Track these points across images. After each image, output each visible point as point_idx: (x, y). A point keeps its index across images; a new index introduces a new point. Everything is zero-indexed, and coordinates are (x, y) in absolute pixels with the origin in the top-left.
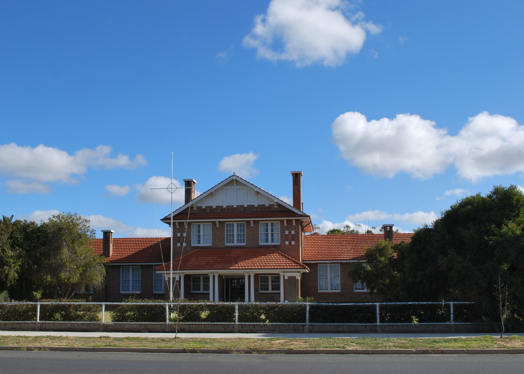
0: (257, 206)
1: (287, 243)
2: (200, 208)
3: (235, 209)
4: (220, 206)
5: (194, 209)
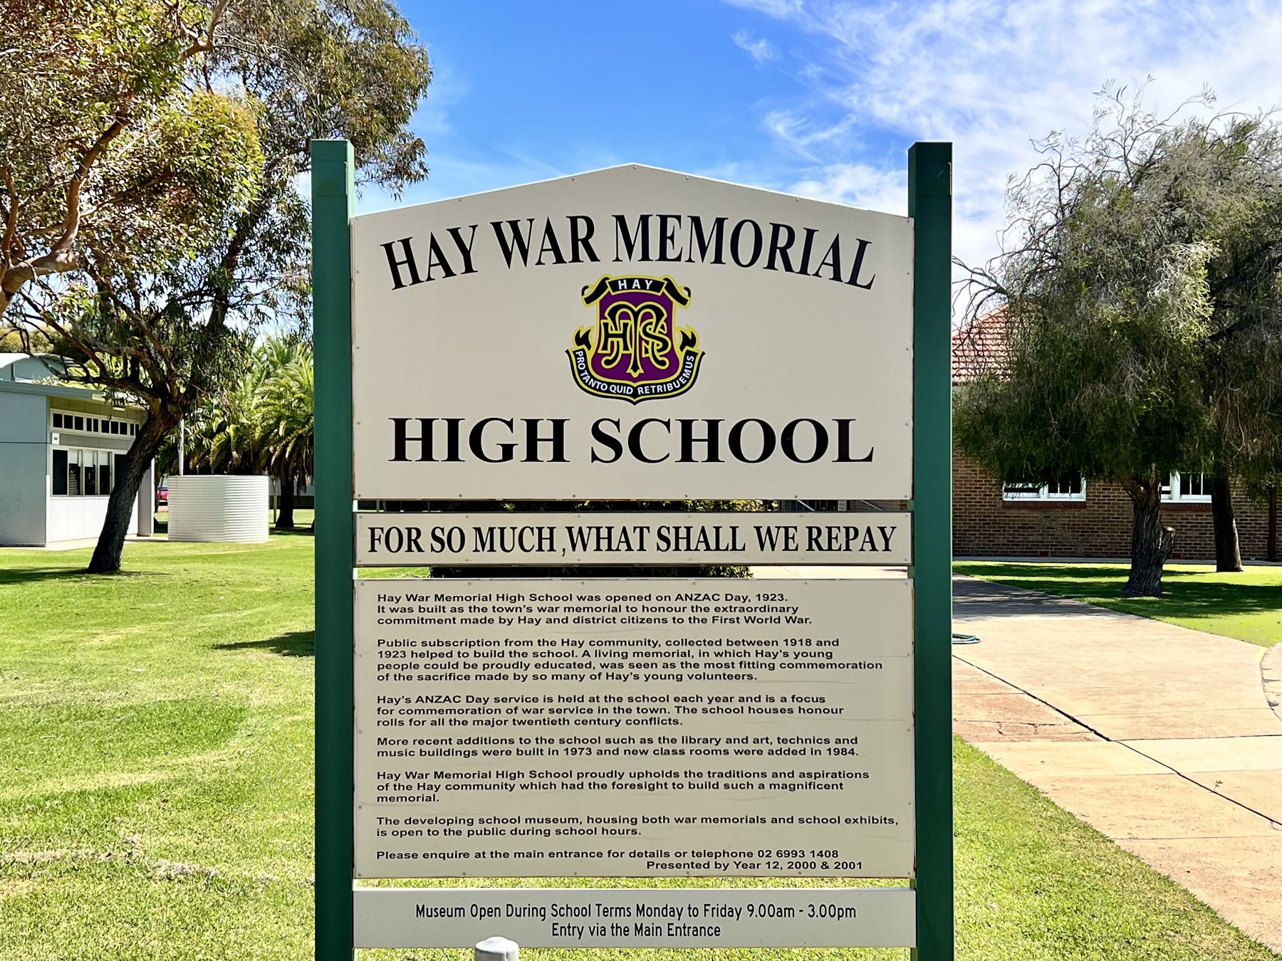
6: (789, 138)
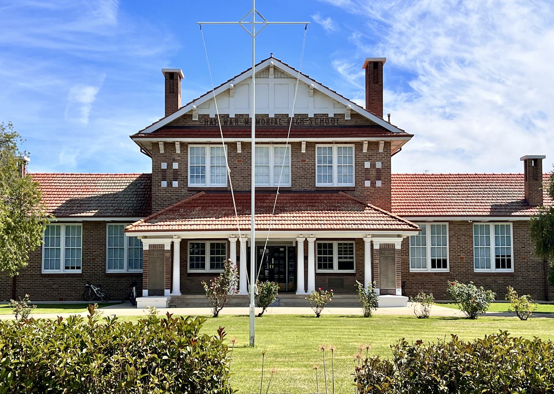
0: (234, 117)
1: (367, 184)
2: (204, 117)
3: (272, 121)
4: (242, 115)
5: (193, 119)
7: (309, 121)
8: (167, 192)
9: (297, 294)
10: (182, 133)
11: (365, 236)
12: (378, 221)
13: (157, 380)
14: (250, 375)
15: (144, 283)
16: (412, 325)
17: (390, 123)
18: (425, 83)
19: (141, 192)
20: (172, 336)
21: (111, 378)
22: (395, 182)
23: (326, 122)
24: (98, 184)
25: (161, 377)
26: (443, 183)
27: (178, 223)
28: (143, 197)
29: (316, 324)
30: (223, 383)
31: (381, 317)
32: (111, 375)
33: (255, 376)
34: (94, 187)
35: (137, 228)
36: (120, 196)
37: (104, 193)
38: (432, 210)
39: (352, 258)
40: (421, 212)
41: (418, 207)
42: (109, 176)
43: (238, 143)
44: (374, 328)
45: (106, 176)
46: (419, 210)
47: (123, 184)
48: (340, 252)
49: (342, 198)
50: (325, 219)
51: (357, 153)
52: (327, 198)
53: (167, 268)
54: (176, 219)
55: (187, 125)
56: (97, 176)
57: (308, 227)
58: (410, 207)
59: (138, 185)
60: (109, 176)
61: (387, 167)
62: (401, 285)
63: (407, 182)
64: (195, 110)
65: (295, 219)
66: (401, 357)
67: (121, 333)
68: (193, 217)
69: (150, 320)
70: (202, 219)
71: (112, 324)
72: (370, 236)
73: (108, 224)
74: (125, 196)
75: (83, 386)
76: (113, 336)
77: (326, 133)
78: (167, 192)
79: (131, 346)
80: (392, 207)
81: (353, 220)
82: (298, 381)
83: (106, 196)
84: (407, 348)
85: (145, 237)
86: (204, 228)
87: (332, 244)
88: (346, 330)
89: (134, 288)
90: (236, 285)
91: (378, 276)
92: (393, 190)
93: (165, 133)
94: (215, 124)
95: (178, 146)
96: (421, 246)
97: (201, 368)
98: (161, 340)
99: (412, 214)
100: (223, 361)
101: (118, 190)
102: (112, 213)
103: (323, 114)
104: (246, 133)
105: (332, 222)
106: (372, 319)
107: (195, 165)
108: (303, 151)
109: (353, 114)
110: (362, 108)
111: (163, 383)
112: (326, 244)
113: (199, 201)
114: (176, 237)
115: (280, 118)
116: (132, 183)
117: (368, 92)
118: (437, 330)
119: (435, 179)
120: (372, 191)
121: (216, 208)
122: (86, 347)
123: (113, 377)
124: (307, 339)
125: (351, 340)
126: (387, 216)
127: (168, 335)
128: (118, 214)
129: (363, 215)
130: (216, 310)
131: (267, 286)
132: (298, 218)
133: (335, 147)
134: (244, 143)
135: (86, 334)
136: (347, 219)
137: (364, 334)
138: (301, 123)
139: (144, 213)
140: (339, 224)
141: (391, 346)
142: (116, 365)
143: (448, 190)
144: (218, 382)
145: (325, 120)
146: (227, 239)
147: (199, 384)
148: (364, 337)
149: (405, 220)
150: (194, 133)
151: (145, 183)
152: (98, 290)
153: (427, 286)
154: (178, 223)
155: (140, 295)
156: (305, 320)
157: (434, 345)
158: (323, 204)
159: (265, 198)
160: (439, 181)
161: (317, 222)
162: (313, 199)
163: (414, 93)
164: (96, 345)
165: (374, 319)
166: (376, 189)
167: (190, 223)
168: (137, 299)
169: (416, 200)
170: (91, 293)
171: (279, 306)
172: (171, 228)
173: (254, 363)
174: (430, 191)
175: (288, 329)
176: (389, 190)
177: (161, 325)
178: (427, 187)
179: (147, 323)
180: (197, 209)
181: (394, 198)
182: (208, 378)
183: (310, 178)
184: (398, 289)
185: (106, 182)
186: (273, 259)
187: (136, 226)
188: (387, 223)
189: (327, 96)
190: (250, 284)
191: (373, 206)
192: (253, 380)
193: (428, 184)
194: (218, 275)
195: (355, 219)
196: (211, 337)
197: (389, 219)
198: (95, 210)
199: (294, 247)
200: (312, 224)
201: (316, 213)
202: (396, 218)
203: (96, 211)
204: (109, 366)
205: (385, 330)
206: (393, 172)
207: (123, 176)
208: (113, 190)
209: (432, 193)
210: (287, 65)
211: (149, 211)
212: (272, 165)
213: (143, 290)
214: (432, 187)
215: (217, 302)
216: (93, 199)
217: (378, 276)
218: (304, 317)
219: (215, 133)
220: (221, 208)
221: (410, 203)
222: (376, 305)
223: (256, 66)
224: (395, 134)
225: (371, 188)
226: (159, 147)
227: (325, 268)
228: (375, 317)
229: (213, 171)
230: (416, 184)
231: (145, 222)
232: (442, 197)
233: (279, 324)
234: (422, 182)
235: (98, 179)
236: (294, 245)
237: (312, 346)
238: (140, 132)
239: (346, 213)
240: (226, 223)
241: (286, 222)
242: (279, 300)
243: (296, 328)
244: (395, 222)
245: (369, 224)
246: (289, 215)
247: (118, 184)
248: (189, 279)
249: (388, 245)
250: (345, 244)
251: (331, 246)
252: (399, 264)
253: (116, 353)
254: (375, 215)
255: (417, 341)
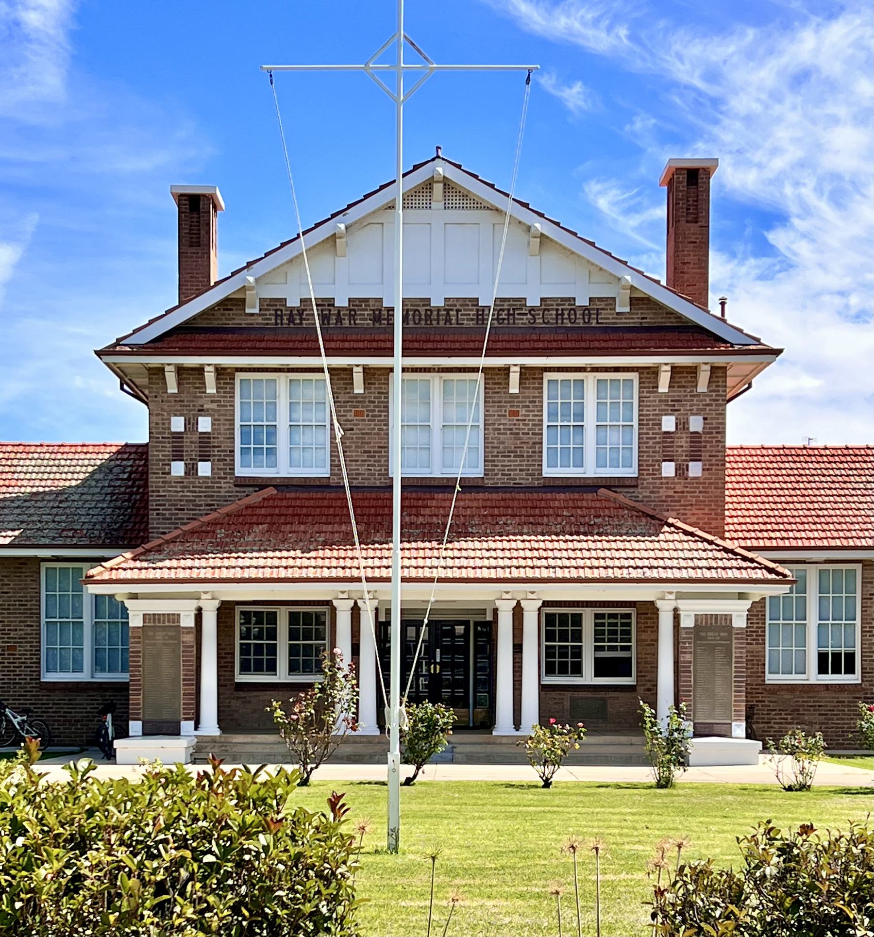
1: (668, 469)
2: (275, 305)
3: (438, 315)
4: (366, 300)
5: (248, 311)
6: (615, 216)
7: (529, 316)
8: (186, 487)
9: (494, 733)
10: (221, 344)
11: (660, 596)
12: (692, 559)
13: (191, 910)
14: (393, 914)
15: (133, 704)
16: (771, 805)
17: (724, 321)
18: (804, 236)
19: (123, 489)
20: (223, 810)
21: (83, 904)
22: (735, 466)
23: (570, 319)
24: (19, 469)
25: (199, 903)
26: (851, 469)
27: (211, 563)
28: (129, 500)
29: (541, 803)
30: (342, 921)
31: (696, 788)
32: (84, 896)
33: (404, 916)
34: (9, 476)
35: (114, 575)
36: (72, 498)
37: (34, 490)
38: (823, 535)
39: (628, 648)
40: (796, 538)
41: (788, 527)
42: (45, 449)
43: (355, 369)
44: (681, 811)
45: (39, 450)
46: (791, 534)
47: (78, 469)
48: (599, 635)
49: (607, 504)
50: (565, 554)
51: (645, 394)
52: (571, 504)
53: (188, 670)
54: (208, 553)
55: (231, 324)
56: (15, 449)
57: (523, 575)
58: (769, 527)
59: (116, 470)
60: (45, 449)
61: (716, 429)
62: (744, 713)
63: (764, 465)
64: (251, 288)
65: (493, 553)
66: (763, 862)
67: (105, 802)
68: (248, 548)
69: (169, 775)
70: (270, 554)
71: (82, 781)
72: (673, 597)
73: (44, 566)
74: (84, 497)
75: (17, 922)
76: (88, 807)
77: (569, 345)
78: (186, 487)
79: (128, 833)
80: (726, 528)
81: (633, 559)
82: (506, 930)
83: (39, 498)
84: (778, 844)
85: (134, 596)
86: (275, 576)
87: (581, 615)
88: (616, 817)
89: (109, 717)
90: (353, 710)
91: (690, 691)
92: (730, 486)
93: (180, 344)
94: (301, 324)
95: (210, 377)
96: (794, 622)
97: (294, 886)
98: (198, 820)
99: (774, 543)
100: (343, 869)
101: (67, 483)
102: (54, 538)
103: (563, 299)
104: (374, 345)
105: (581, 563)
106: (675, 792)
107: (252, 423)
108: (514, 389)
109: (637, 299)
110: (658, 282)
111: (205, 918)
112: (566, 615)
113: (263, 511)
114: (208, 596)
115: (458, 307)
116: (100, 466)
117: (672, 243)
118: (832, 818)
119: (831, 459)
120: (679, 488)
121: (302, 528)
122: (24, 832)
123: (89, 902)
124: (523, 837)
125: (626, 840)
126: (714, 547)
127: (215, 807)
128: (69, 540)
129: (657, 545)
130: (305, 769)
131: (426, 713)
132: (500, 554)
133: (590, 380)
134: (370, 369)
135: (24, 803)
136: (617, 554)
137: (658, 825)
138: (508, 319)
139: (131, 539)
140: (597, 568)
141: (738, 839)
142: (95, 874)
143: (862, 486)
144: (330, 918)
145: (566, 312)
146: (328, 603)
147: (288, 921)
148: (657, 832)
149: (760, 557)
150: (249, 344)
151: (131, 466)
152: (23, 721)
153: (806, 718)
154: (211, 563)
155: (123, 733)
156: (516, 792)
157: (841, 837)
158: (559, 519)
159: (420, 503)
160: (841, 462)
161: (544, 563)
162: (536, 507)
163: (779, 259)
164: (46, 829)
165: (681, 792)
166: (689, 483)
167: (240, 562)
168: (117, 744)
169: (784, 509)
170: (6, 728)
171: (452, 761)
172: (195, 574)
173: (400, 888)
174: (818, 489)
175: (476, 814)
176: (720, 485)
177: (198, 785)
178: (811, 479)
179: (163, 780)
180: (256, 529)
181: (731, 506)
182: (308, 908)
183: (531, 456)
184: (738, 723)
185: (39, 462)
186: (438, 650)
187: (112, 569)
188: (713, 564)
189: (573, 253)
190: (389, 706)
191: (680, 524)
192: (400, 926)
193: (814, 472)
194: (311, 686)
195: (637, 554)
196: (314, 815)
197: (719, 555)
198: (13, 530)
199: (489, 623)
200: (532, 568)
201: (544, 541)
202: (736, 554)
203: (17, 533)
204: (78, 878)
205: (707, 817)
206: (731, 440)
207: (79, 449)
208: (56, 483)
209: (822, 492)
210: (476, 177)
211: (142, 534)
212: (436, 423)
213: (131, 723)
214: (823, 479)
215: (306, 751)
216: (8, 503)
217: (690, 691)
218: (512, 786)
219: (299, 345)
220: (316, 528)
221: (769, 517)
222: (682, 761)
223: (404, 175)
224: (736, 348)
225: (676, 480)
226: (164, 378)
227: (563, 671)
228: (684, 788)
229: (296, 438)
230: (784, 472)
231: (134, 559)
232: (848, 502)
233: (456, 801)
234: (799, 465)
235: (19, 456)
236: (489, 618)
237: (532, 851)
238: (118, 342)
239: (615, 541)
240: (327, 563)
241: (471, 563)
242: (453, 747)
243: (495, 812)
244: (734, 563)
245: (671, 568)
246: (478, 545)
247: (66, 469)
248: (238, 698)
249: (716, 619)
250: (611, 616)
251: (577, 620)
252: (742, 662)
253: (95, 846)
254: (686, 545)
255: (802, 827)
